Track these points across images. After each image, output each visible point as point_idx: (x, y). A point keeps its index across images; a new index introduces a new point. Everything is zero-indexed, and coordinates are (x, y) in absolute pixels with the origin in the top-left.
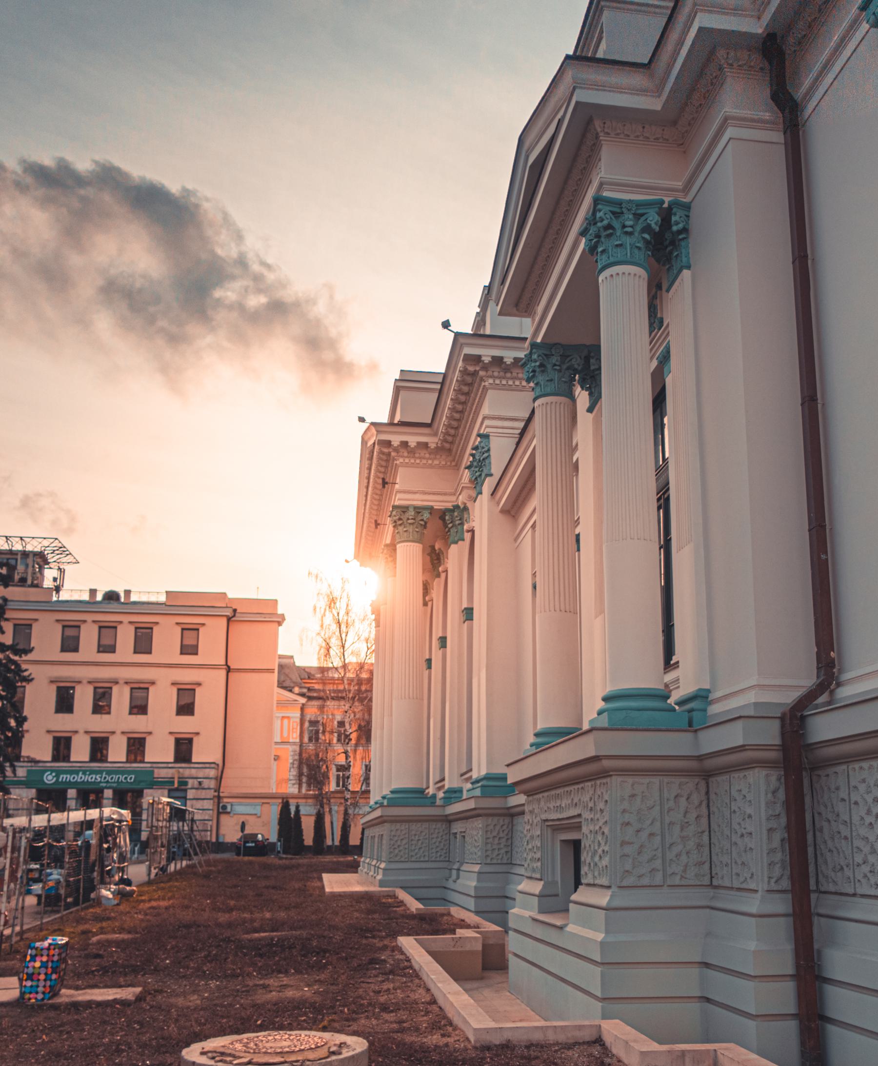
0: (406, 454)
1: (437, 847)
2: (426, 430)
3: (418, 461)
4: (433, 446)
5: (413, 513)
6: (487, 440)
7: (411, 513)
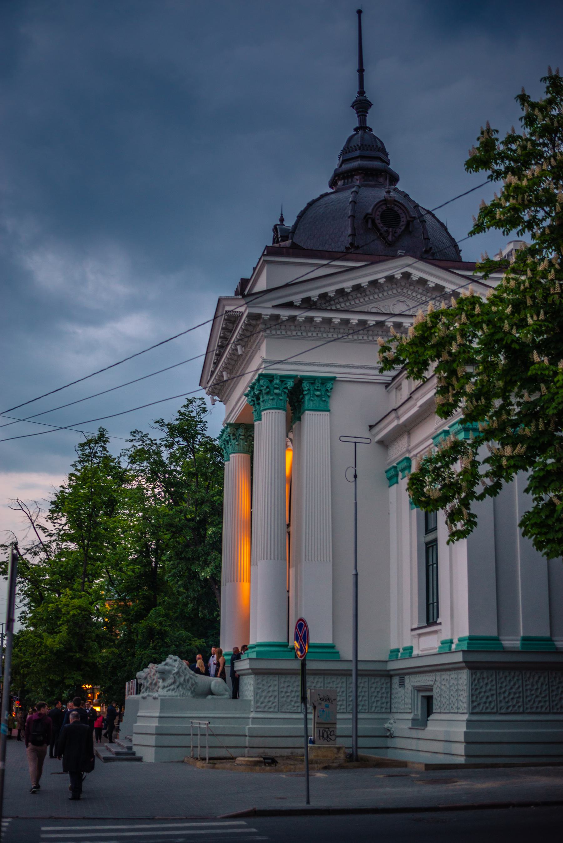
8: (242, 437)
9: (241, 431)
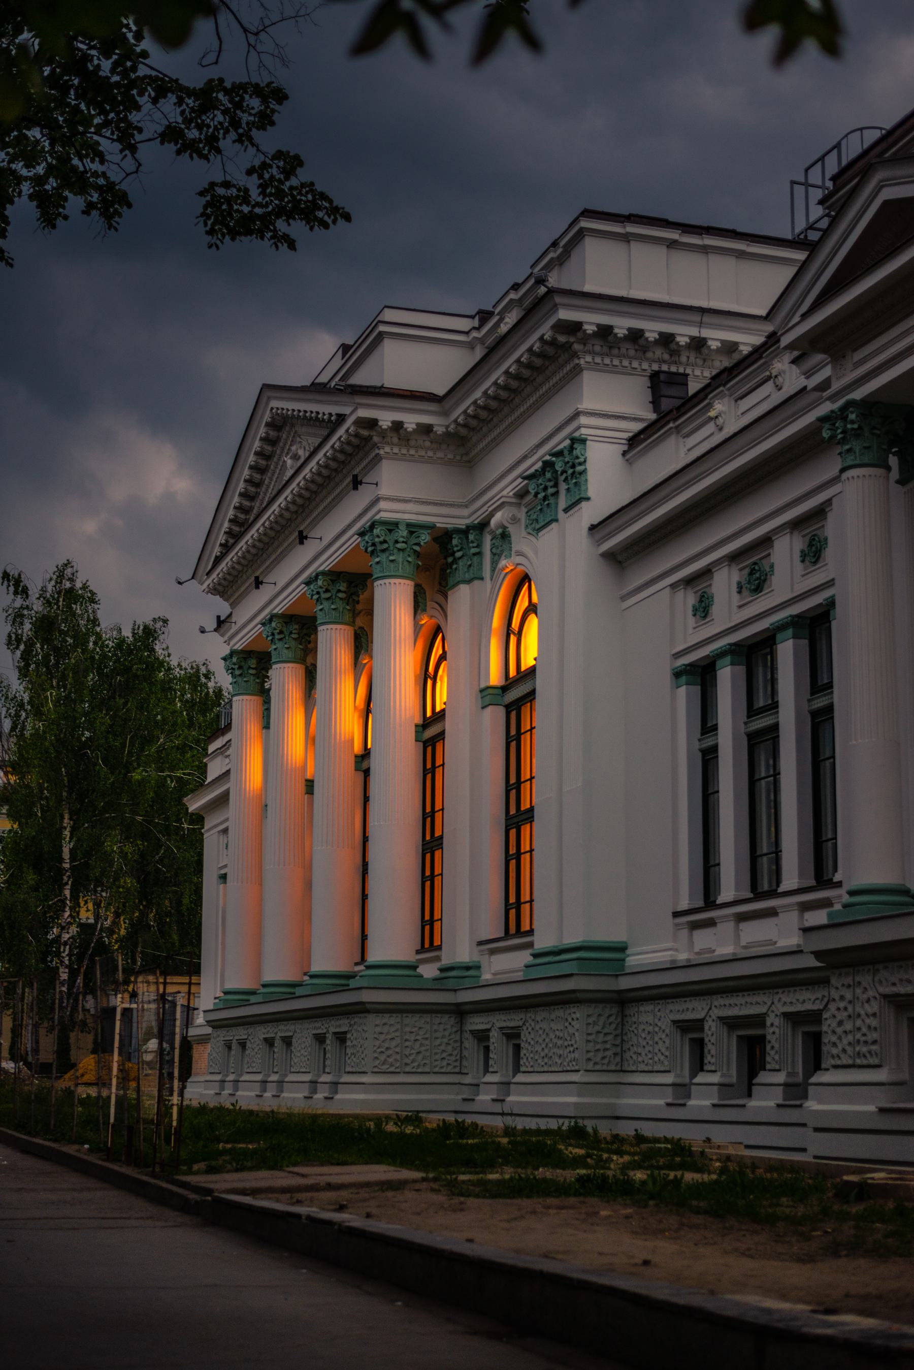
0: (395, 440)
1: (444, 1051)
2: (433, 407)
3: (412, 452)
4: (440, 430)
5: (405, 533)
6: (582, 446)
7: (403, 532)
8: (341, 595)
9: (253, 662)
